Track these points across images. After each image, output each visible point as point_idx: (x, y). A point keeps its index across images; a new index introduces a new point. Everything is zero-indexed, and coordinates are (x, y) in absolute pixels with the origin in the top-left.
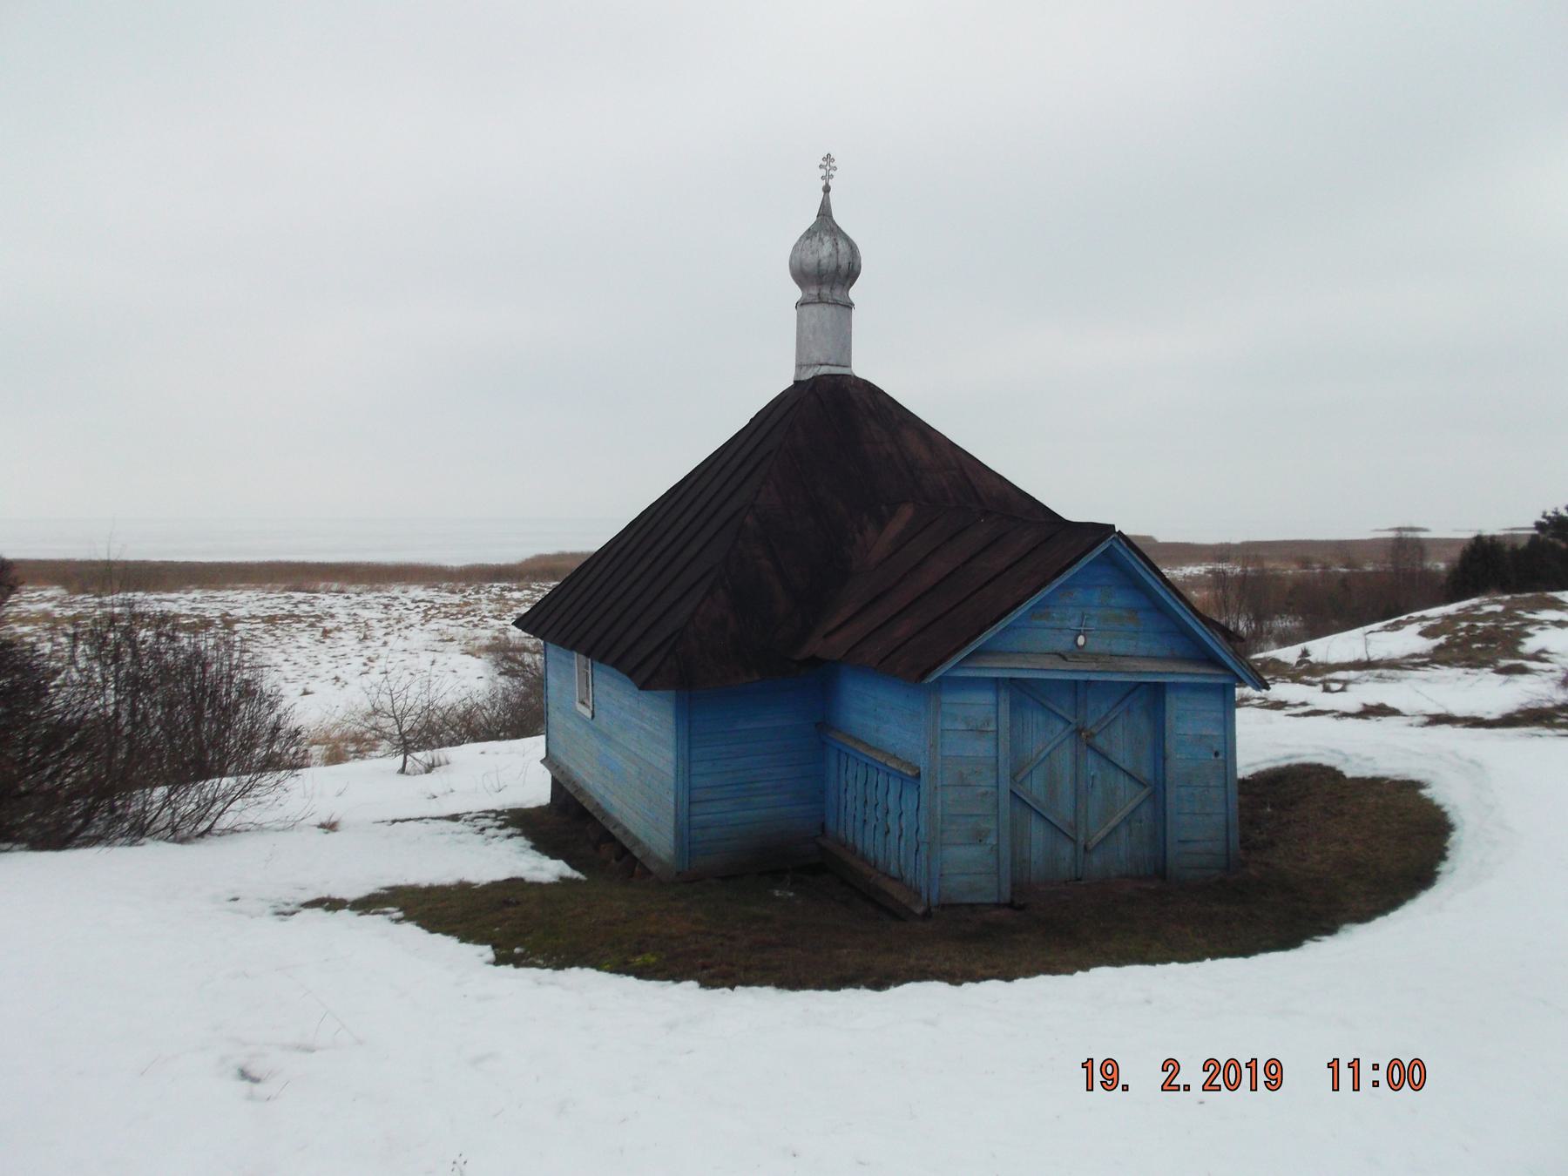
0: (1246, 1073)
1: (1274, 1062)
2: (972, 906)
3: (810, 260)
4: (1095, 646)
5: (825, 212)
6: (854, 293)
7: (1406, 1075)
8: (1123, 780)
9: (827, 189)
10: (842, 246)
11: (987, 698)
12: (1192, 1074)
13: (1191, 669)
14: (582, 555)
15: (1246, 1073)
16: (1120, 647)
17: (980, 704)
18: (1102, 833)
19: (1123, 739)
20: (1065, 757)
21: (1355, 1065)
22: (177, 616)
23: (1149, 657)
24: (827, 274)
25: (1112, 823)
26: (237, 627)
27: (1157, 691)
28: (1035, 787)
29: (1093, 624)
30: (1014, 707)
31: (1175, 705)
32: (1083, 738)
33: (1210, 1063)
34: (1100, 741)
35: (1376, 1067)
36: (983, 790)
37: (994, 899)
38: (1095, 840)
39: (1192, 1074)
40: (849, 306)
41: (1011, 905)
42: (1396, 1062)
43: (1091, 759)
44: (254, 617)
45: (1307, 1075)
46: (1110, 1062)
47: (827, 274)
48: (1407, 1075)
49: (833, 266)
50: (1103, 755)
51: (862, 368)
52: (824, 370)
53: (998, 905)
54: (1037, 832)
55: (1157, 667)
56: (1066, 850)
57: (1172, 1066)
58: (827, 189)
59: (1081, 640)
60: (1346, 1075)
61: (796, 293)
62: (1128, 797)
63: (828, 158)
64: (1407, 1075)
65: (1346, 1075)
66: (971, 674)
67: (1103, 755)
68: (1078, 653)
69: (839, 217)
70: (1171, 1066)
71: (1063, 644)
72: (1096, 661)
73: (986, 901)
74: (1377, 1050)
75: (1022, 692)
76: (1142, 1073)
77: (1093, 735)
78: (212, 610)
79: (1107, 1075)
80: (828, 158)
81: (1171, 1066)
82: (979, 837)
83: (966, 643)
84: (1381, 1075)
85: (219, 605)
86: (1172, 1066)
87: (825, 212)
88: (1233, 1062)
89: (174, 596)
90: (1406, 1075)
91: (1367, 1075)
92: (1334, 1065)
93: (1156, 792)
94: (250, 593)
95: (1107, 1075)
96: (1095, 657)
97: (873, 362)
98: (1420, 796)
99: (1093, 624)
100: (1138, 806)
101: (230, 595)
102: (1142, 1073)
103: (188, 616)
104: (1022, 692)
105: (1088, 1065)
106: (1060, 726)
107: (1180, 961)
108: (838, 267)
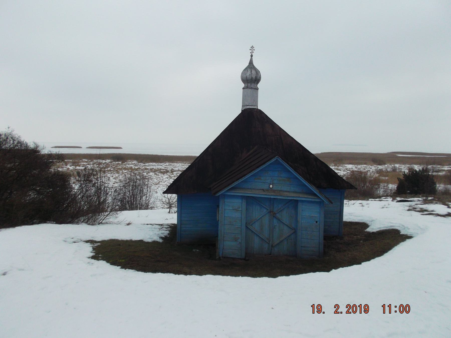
0: (358, 308)
1: (366, 305)
2: (233, 259)
3: (245, 76)
4: (275, 188)
5: (251, 62)
6: (259, 86)
7: (405, 309)
8: (285, 228)
9: (252, 56)
10: (254, 72)
11: (240, 201)
12: (343, 309)
13: (306, 196)
14: (195, 157)
15: (358, 308)
16: (285, 188)
17: (237, 203)
18: (278, 242)
19: (285, 216)
20: (266, 220)
21: (390, 306)
22: (161, 169)
23: (294, 192)
24: (251, 79)
25: (281, 239)
26: (174, 173)
27: (295, 203)
28: (256, 227)
29: (275, 182)
30: (247, 205)
31: (301, 207)
32: (273, 214)
33: (348, 306)
34: (278, 215)
35: (396, 307)
36: (237, 226)
37: (240, 257)
38: (275, 244)
39: (343, 309)
40: (257, 89)
41: (245, 259)
42: (401, 305)
43: (275, 221)
44: (179, 170)
45: (376, 309)
46: (319, 305)
47: (251, 79)
48: (405, 309)
49: (250, 78)
50: (279, 220)
51: (259, 108)
52: (248, 107)
53: (241, 259)
54: (257, 241)
55: (297, 195)
56: (266, 246)
57: (337, 306)
58: (252, 56)
59: (271, 186)
60: (387, 309)
61: (243, 85)
62: (287, 232)
63: (252, 47)
64: (405, 309)
65: (387, 309)
66: (232, 194)
67: (279, 220)
68: (269, 190)
69: (255, 64)
70: (337, 306)
71: (265, 187)
72: (274, 192)
73: (237, 257)
74: (396, 302)
75: (250, 201)
76: (328, 308)
77: (275, 214)
78: (169, 168)
79: (318, 309)
80: (252, 47)
81: (337, 306)
82: (236, 240)
83: (229, 185)
84: (397, 309)
85: (172, 167)
86: (337, 306)
87: (251, 62)
88: (355, 305)
89: (162, 164)
90: (405, 309)
91: (393, 309)
92: (384, 306)
93: (295, 231)
94: (180, 164)
95: (318, 309)
96: (274, 191)
97: (262, 106)
98: (369, 233)
99: (275, 182)
100: (291, 235)
101: (175, 164)
102: (328, 308)
103: (163, 169)
104: (250, 201)
105: (313, 306)
106: (265, 210)
107: (231, 276)
108: (252, 78)
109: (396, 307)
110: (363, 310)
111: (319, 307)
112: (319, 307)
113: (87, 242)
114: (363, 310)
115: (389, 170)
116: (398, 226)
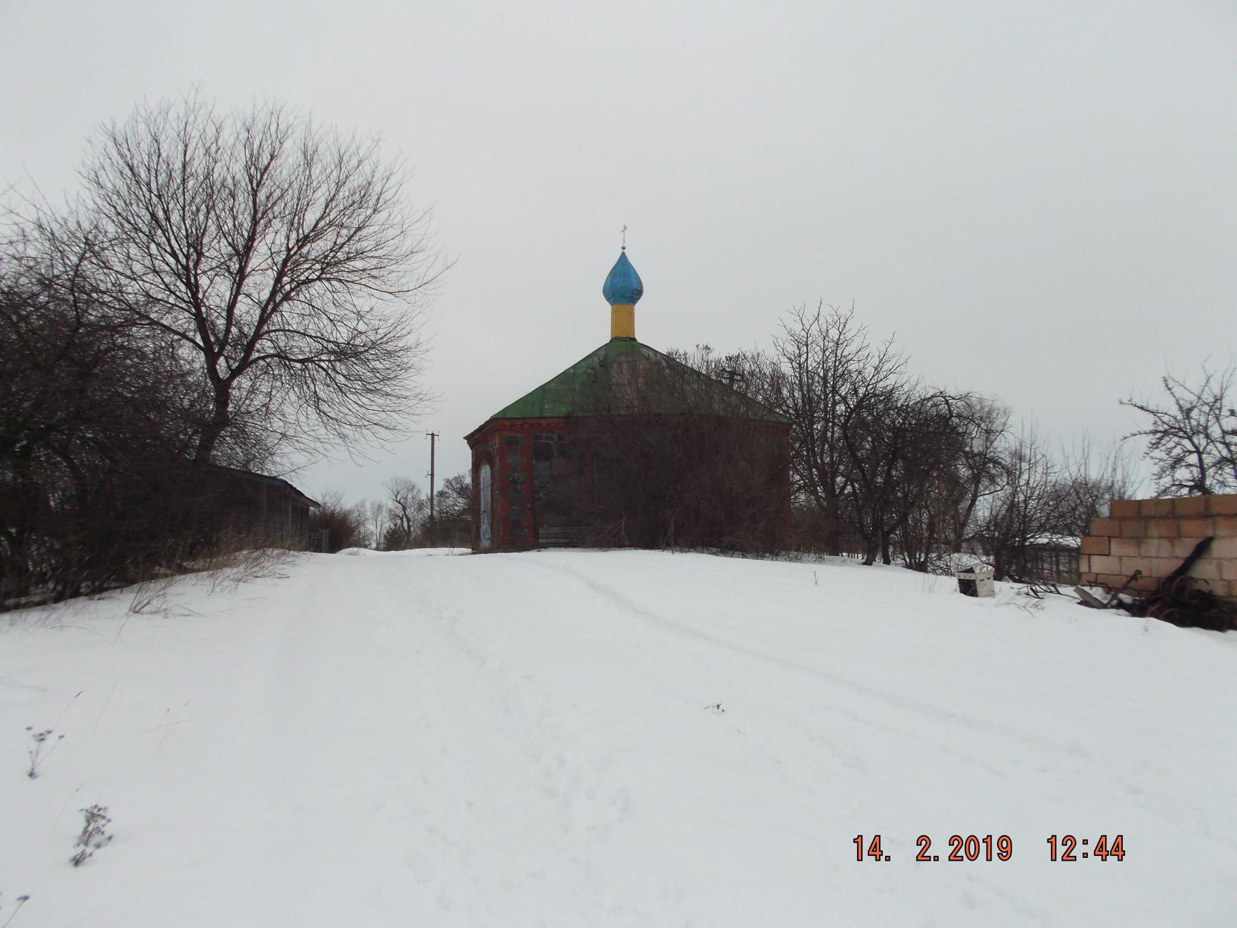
0: (983, 846)
12: (940, 847)
15: (983, 846)
24: (623, 289)
33: (954, 839)
39: (940, 847)
47: (623, 289)
57: (924, 841)
70: (924, 841)
81: (924, 841)
86: (924, 841)
88: (972, 838)
110: (995, 850)
111: (1004, 844)
112: (1004, 844)
114: (995, 850)
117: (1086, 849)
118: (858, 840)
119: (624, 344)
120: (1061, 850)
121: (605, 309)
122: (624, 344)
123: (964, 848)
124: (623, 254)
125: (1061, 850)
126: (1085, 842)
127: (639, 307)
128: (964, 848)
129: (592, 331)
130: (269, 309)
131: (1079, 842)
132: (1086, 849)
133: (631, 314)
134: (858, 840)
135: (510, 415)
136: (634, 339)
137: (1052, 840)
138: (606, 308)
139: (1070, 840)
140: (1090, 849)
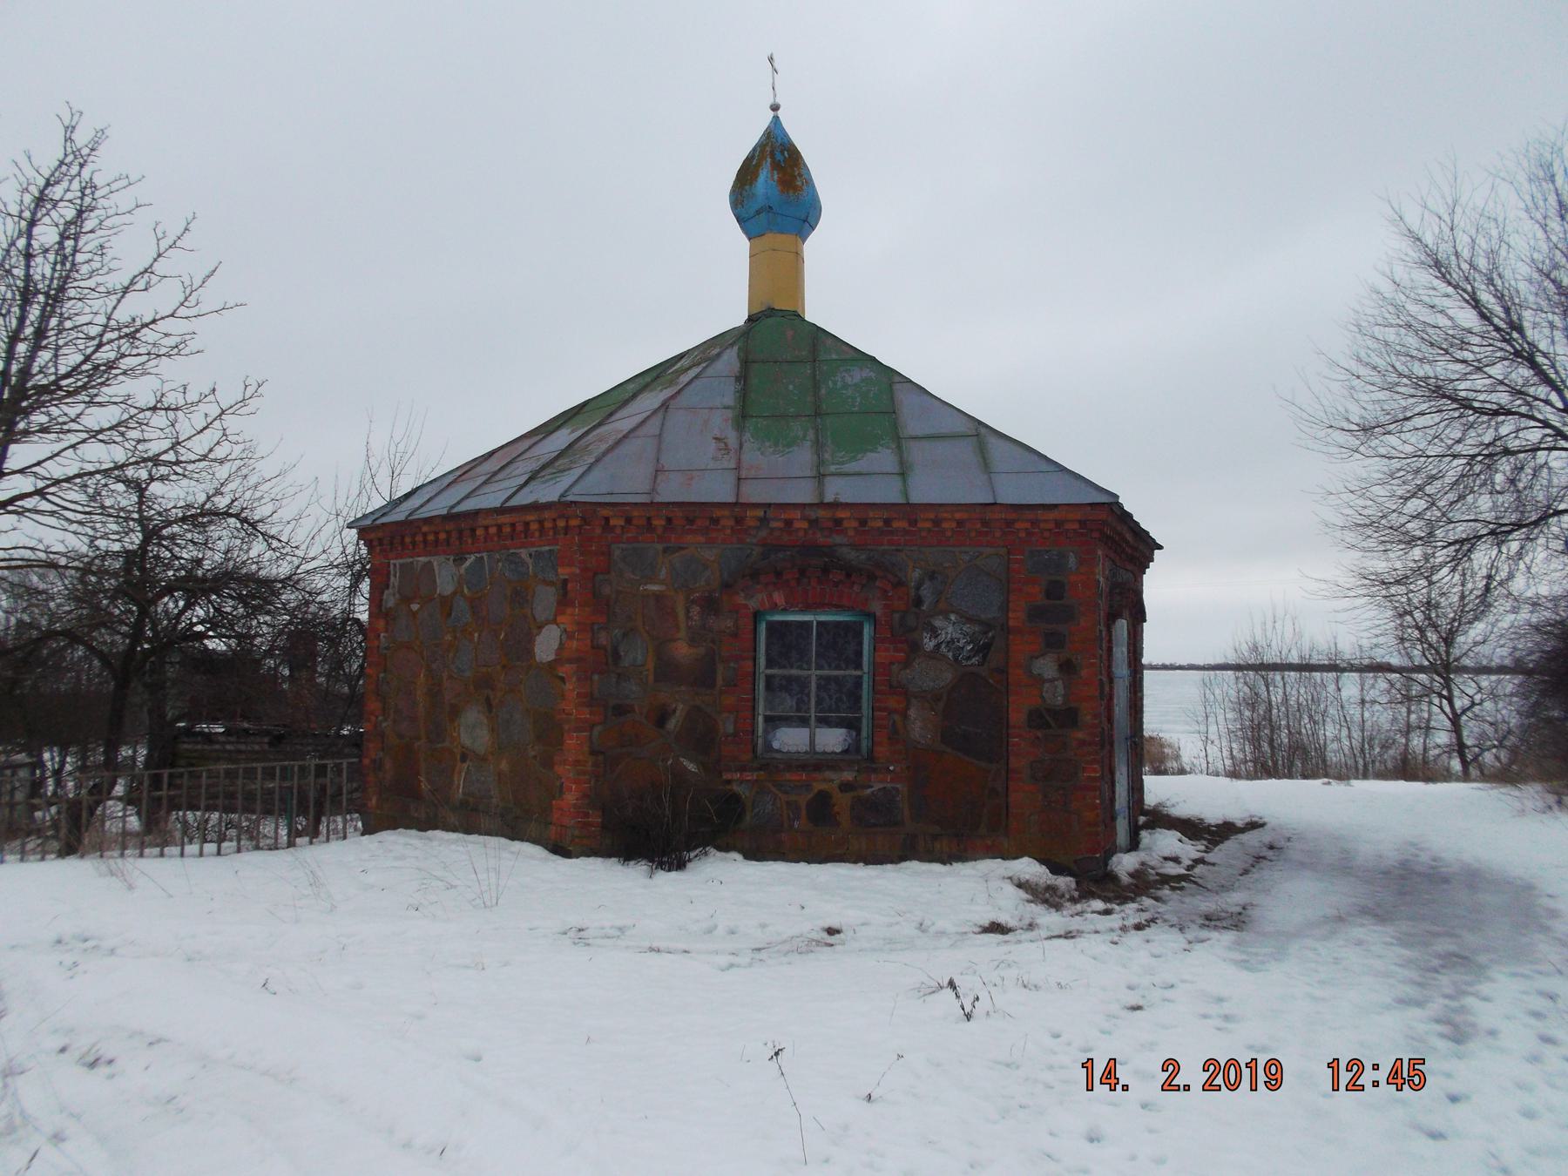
0: (1246, 1072)
12: (1192, 1074)
15: (1246, 1072)
24: (774, 190)
33: (1210, 1064)
39: (1192, 1074)
45: (1306, 1072)
47: (774, 190)
48: (478, 1059)
57: (1172, 1066)
70: (1171, 1066)
81: (1171, 1066)
86: (1172, 1066)
88: (1233, 1062)
102: (1142, 1071)
109: (1376, 1067)
110: (1262, 1078)
111: (1273, 1070)
112: (1273, 1070)
113: (1020, 885)
114: (1262, 1078)
115: (108, 824)
116: (532, 857)
117: (1376, 1075)
118: (1088, 1065)
119: (781, 363)
120: (1345, 1077)
121: (733, 247)
122: (781, 363)
123: (1222, 1075)
124: (776, 118)
125: (1345, 1077)
126: (1376, 1067)
127: (813, 247)
128: (1222, 1075)
129: (709, 291)
130: (1448, 653)
131: (1368, 1067)
132: (1376, 1075)
133: (798, 256)
134: (1088, 1065)
135: (620, 480)
136: (797, 316)
137: (1333, 1065)
138: (738, 244)
139: (1356, 1065)
140: (1382, 1075)
